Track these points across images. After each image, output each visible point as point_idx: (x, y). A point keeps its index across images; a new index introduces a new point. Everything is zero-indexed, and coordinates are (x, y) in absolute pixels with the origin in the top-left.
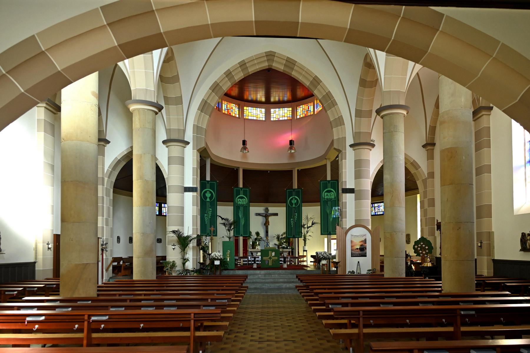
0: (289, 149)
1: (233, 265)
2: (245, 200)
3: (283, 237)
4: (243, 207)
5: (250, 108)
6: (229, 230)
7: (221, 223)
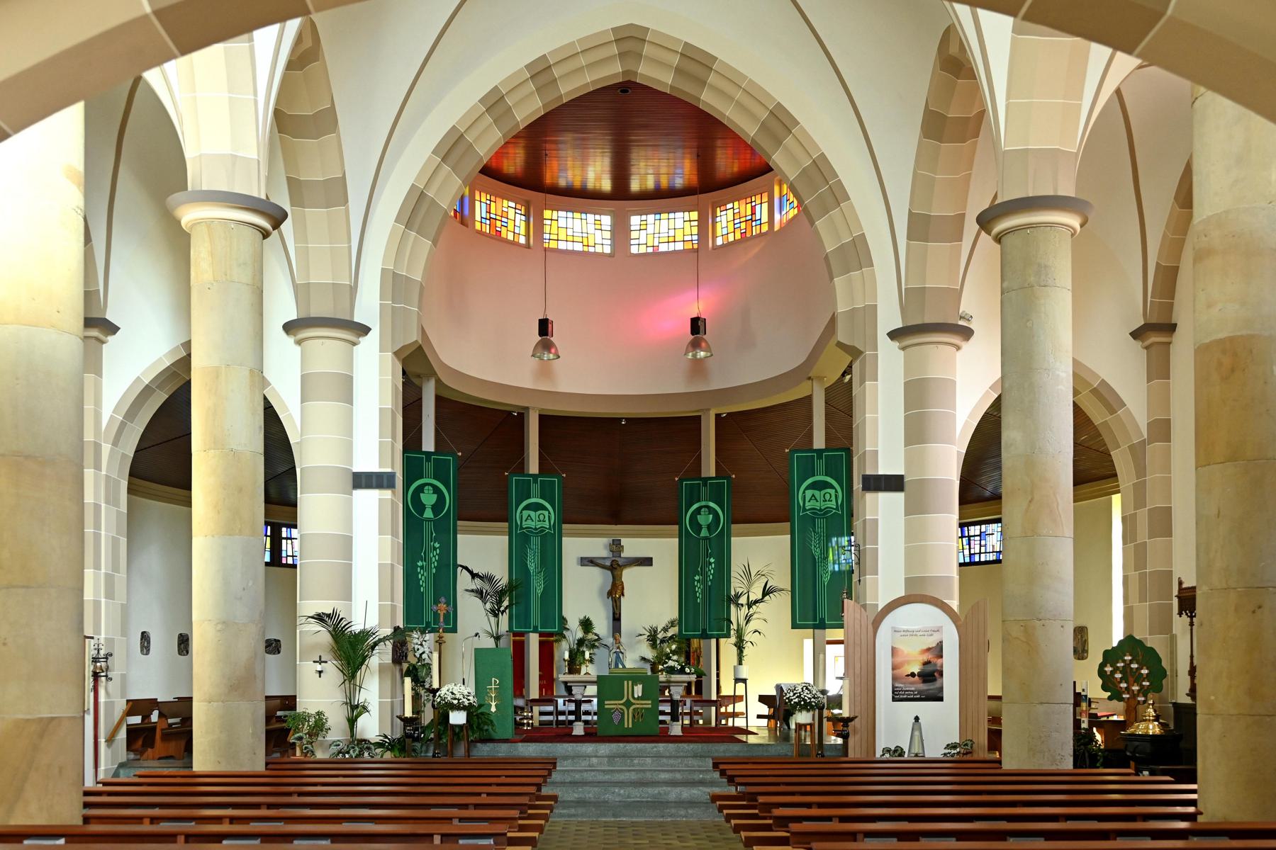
0: (690, 348)
3: (669, 634)
5: (562, 214)
6: (495, 613)
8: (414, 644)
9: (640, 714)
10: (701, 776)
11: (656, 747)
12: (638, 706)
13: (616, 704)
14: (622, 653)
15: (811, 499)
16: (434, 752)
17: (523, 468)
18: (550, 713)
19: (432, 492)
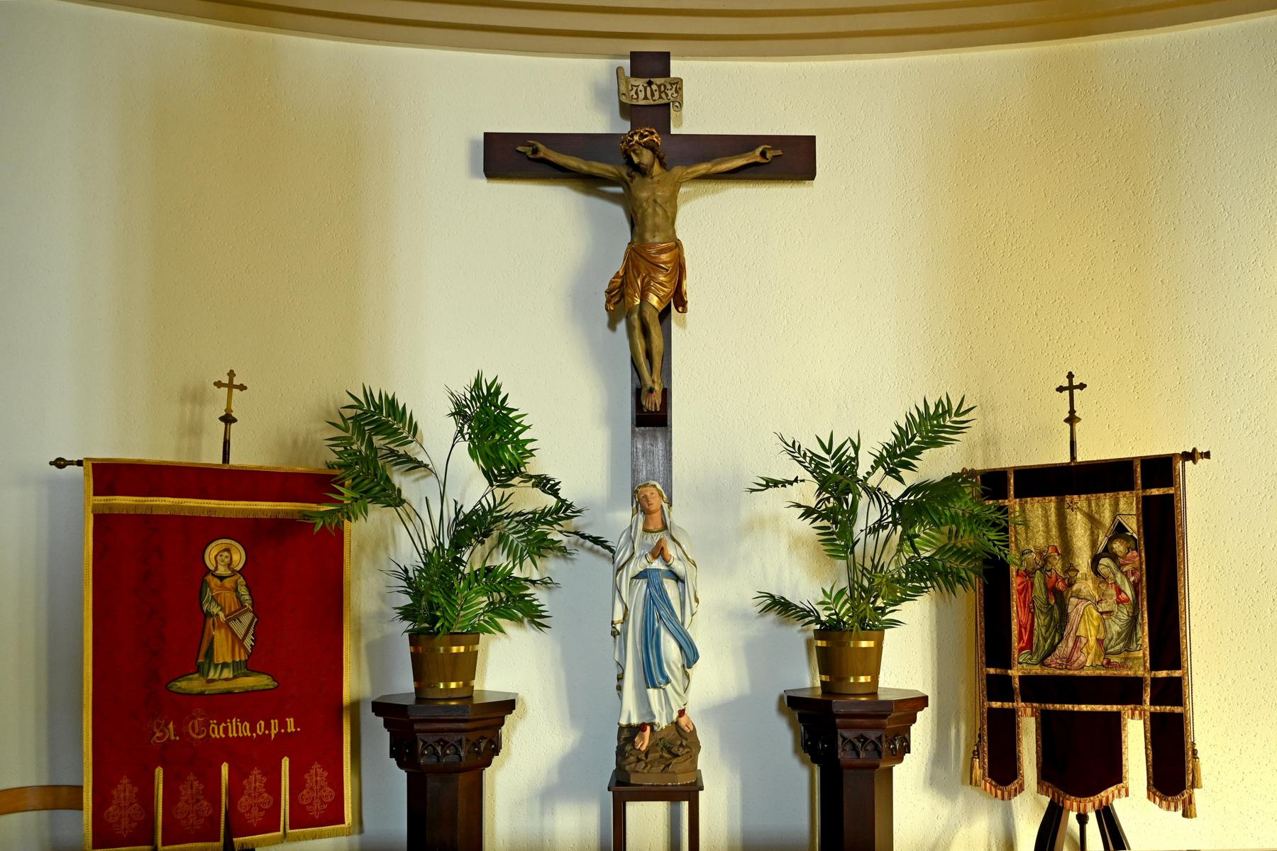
14: (678, 579)
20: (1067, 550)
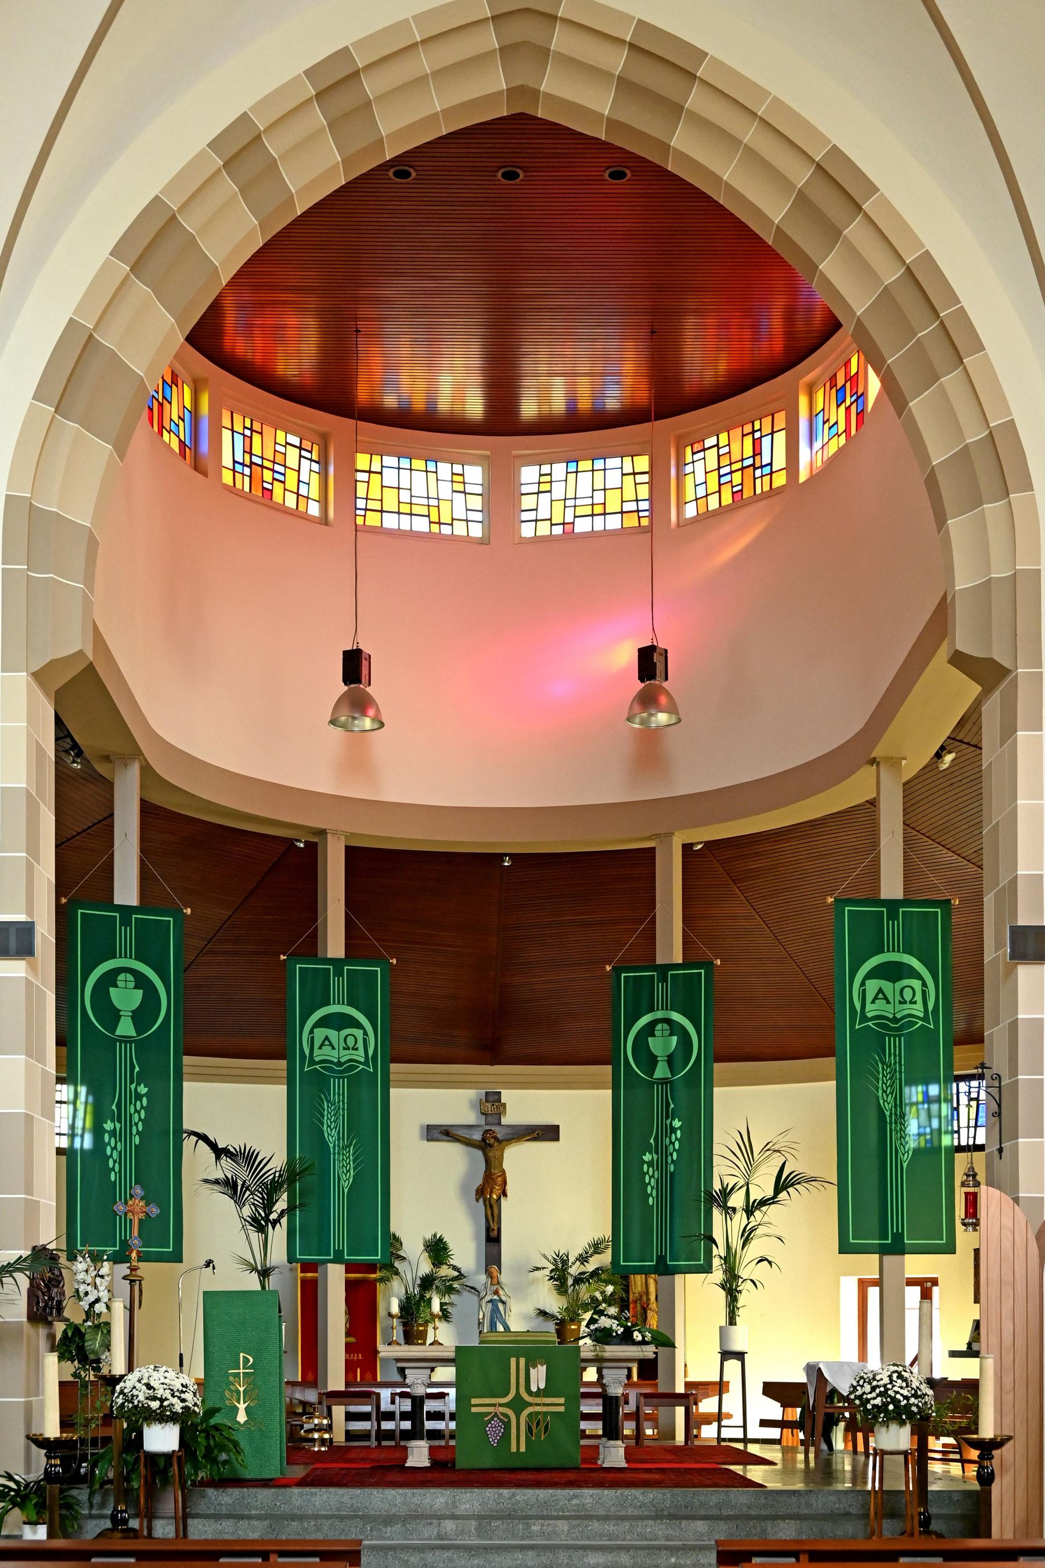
0: (637, 708)
1: (276, 1445)
2: (359, 1033)
3: (590, 1267)
4: (349, 1077)
5: (390, 461)
6: (260, 1224)
7: (212, 1177)
8: (78, 1282)
9: (542, 1425)
10: (673, 1560)
11: (576, 1497)
12: (538, 1409)
13: (494, 1405)
14: (504, 1303)
15: (876, 998)
16: (115, 1509)
17: (315, 945)
18: (365, 1417)
19: (133, 985)
20: (647, 1293)
